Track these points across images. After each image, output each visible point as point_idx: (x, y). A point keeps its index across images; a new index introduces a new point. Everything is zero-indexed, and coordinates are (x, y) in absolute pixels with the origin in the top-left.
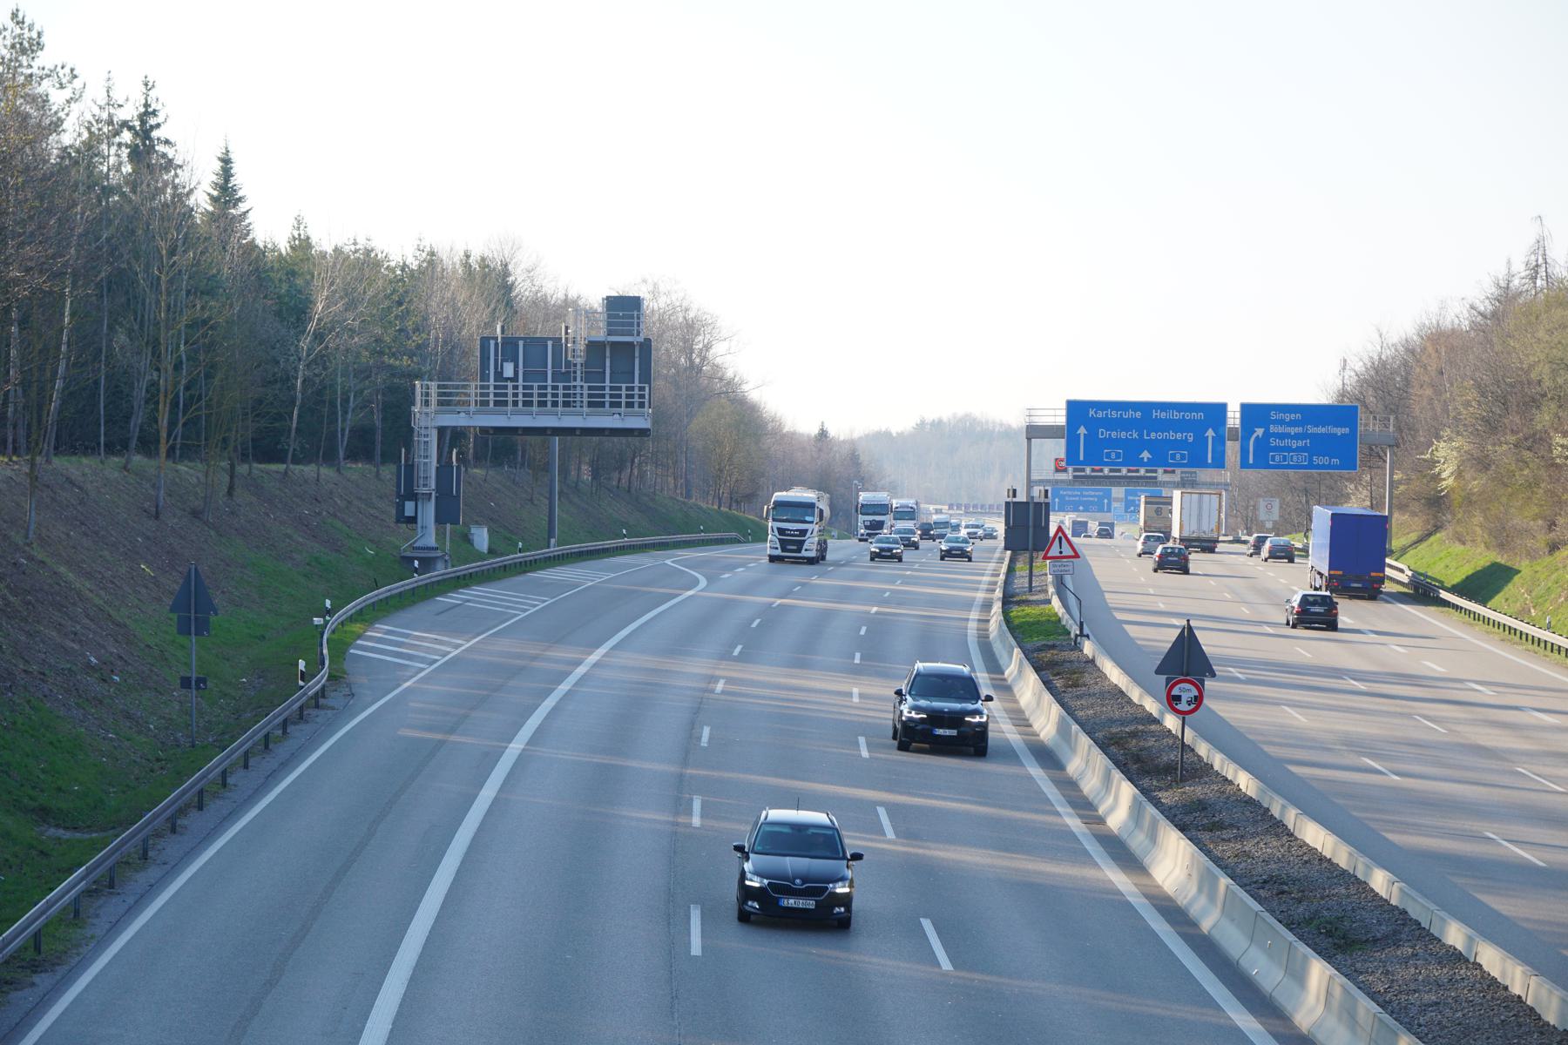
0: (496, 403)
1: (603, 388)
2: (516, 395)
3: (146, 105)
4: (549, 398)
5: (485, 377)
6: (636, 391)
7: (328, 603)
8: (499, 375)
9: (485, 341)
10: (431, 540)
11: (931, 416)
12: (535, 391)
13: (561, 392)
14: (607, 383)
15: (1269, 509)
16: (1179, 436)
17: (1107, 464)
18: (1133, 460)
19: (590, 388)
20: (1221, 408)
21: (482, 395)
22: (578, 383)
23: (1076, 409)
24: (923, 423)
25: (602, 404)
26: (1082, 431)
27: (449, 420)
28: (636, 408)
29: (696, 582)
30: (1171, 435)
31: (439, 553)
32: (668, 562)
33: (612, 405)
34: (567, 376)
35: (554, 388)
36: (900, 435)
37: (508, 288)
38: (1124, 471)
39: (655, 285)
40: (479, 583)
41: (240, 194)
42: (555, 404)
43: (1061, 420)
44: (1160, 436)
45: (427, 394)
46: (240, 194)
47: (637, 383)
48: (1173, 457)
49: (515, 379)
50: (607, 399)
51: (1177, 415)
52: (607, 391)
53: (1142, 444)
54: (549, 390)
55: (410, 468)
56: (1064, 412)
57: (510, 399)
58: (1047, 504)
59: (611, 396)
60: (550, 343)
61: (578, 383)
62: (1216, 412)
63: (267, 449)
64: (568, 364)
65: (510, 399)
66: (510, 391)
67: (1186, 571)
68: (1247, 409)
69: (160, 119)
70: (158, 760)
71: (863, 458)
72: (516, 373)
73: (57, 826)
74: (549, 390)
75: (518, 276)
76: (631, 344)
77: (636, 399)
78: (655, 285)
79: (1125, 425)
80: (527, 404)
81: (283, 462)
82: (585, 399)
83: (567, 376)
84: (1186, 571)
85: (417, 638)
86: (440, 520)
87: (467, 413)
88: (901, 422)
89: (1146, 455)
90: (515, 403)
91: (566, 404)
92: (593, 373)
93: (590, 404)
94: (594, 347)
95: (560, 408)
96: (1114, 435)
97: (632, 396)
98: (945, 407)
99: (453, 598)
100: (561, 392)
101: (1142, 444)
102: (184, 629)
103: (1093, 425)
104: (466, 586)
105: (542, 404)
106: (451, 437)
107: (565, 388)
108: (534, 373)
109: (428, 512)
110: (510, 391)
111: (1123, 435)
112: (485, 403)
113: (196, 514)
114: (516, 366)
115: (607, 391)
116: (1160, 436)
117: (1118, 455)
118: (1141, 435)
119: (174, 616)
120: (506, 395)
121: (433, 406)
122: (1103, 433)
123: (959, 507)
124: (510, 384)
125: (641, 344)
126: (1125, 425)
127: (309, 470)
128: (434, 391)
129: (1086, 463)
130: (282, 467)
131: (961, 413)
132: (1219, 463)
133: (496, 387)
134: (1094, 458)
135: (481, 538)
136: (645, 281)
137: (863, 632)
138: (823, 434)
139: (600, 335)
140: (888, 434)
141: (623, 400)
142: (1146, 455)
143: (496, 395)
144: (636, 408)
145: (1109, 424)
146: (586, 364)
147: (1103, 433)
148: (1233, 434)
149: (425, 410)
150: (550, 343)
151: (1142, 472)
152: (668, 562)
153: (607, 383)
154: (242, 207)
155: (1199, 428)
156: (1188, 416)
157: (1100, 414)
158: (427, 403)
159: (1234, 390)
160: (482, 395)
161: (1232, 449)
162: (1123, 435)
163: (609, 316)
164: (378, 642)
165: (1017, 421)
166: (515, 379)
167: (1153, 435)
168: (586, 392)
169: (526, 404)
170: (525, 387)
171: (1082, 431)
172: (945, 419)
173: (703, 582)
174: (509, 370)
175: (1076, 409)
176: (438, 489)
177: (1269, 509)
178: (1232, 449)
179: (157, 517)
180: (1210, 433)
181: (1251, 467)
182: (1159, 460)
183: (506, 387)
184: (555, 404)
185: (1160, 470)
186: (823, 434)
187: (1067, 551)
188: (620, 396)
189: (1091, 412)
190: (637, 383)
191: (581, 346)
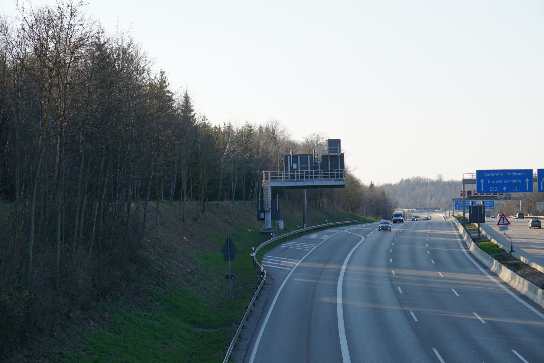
0: (291, 178)
1: (328, 171)
2: (297, 175)
3: (162, 79)
4: (309, 175)
5: (287, 169)
6: (339, 172)
7: (253, 248)
8: (292, 168)
9: (286, 157)
10: (270, 226)
11: (405, 178)
12: (304, 173)
13: (313, 173)
14: (329, 170)
15: (540, 206)
16: (516, 181)
17: (491, 192)
18: (500, 191)
19: (323, 171)
20: (531, 171)
21: (286, 175)
22: (319, 170)
23: (479, 173)
24: (402, 180)
25: (328, 177)
26: (482, 181)
27: (275, 184)
28: (340, 178)
29: (361, 238)
30: (514, 181)
31: (273, 231)
32: (345, 231)
33: (331, 177)
34: (315, 168)
35: (311, 172)
36: (395, 185)
37: (275, 138)
38: (485, 194)
39: (318, 136)
40: (289, 240)
41: (192, 109)
42: (311, 177)
43: (474, 176)
44: (510, 181)
45: (267, 176)
46: (192, 109)
47: (339, 169)
48: (492, 189)
49: (297, 169)
50: (329, 175)
51: (515, 174)
52: (329, 172)
53: (503, 185)
54: (309, 173)
55: (262, 201)
56: (476, 175)
57: (296, 176)
58: (484, 206)
59: (331, 174)
60: (309, 156)
61: (319, 170)
62: (529, 172)
63: (211, 197)
64: (315, 163)
65: (296, 176)
66: (296, 173)
67: (540, 227)
68: (539, 171)
69: (167, 84)
70: (220, 304)
71: (386, 193)
72: (297, 167)
73: (200, 328)
74: (309, 173)
75: (278, 133)
76: (337, 156)
77: (339, 175)
78: (318, 136)
79: (497, 178)
80: (302, 178)
81: (217, 200)
82: (322, 175)
83: (315, 168)
84: (540, 227)
85: (269, 258)
86: (273, 219)
87: (281, 182)
88: (395, 180)
89: (505, 188)
90: (298, 178)
91: (315, 177)
92: (324, 166)
93: (324, 177)
94: (325, 158)
95: (305, 179)
96: (493, 182)
97: (338, 174)
98: (410, 174)
99: (284, 246)
100: (313, 173)
101: (503, 185)
102: (226, 259)
103: (486, 179)
104: (286, 241)
105: (307, 177)
106: (275, 190)
107: (315, 172)
108: (304, 167)
109: (269, 216)
110: (296, 173)
111: (497, 182)
112: (287, 178)
113: (195, 219)
114: (297, 165)
115: (329, 172)
116: (510, 181)
117: (495, 189)
118: (503, 181)
119: (222, 254)
120: (294, 175)
121: (269, 180)
122: (489, 181)
123: (425, 209)
124: (296, 171)
125: (340, 155)
126: (497, 178)
127: (224, 203)
128: (269, 174)
129: (483, 192)
130: (216, 202)
131: (416, 176)
132: (531, 190)
133: (291, 172)
134: (487, 190)
135: (281, 225)
136: (314, 134)
137: (428, 253)
138: (372, 185)
139: (326, 153)
140: (390, 185)
141: (305, 176)
142: (505, 188)
143: (291, 175)
144: (340, 178)
145: (492, 178)
146: (322, 163)
147: (489, 181)
148: (535, 180)
149: (266, 181)
150: (309, 156)
151: (492, 194)
152: (345, 231)
153: (329, 170)
154: (193, 113)
155: (523, 178)
156: (519, 174)
157: (488, 175)
158: (267, 179)
159: (535, 165)
160: (286, 175)
161: (535, 184)
162: (497, 182)
163: (329, 146)
164: (270, 262)
165: (460, 179)
166: (297, 169)
167: (507, 181)
168: (322, 173)
169: (301, 178)
170: (301, 172)
171: (482, 181)
172: (410, 179)
173: (363, 238)
174: (295, 166)
175: (479, 173)
176: (272, 208)
177: (540, 206)
178: (535, 184)
179: (184, 221)
180: (527, 180)
181: (542, 191)
182: (510, 190)
183: (294, 172)
184: (311, 177)
185: (498, 194)
186: (372, 185)
187: (506, 222)
188: (303, 175)
189: (485, 174)
190: (339, 169)
191: (320, 157)
